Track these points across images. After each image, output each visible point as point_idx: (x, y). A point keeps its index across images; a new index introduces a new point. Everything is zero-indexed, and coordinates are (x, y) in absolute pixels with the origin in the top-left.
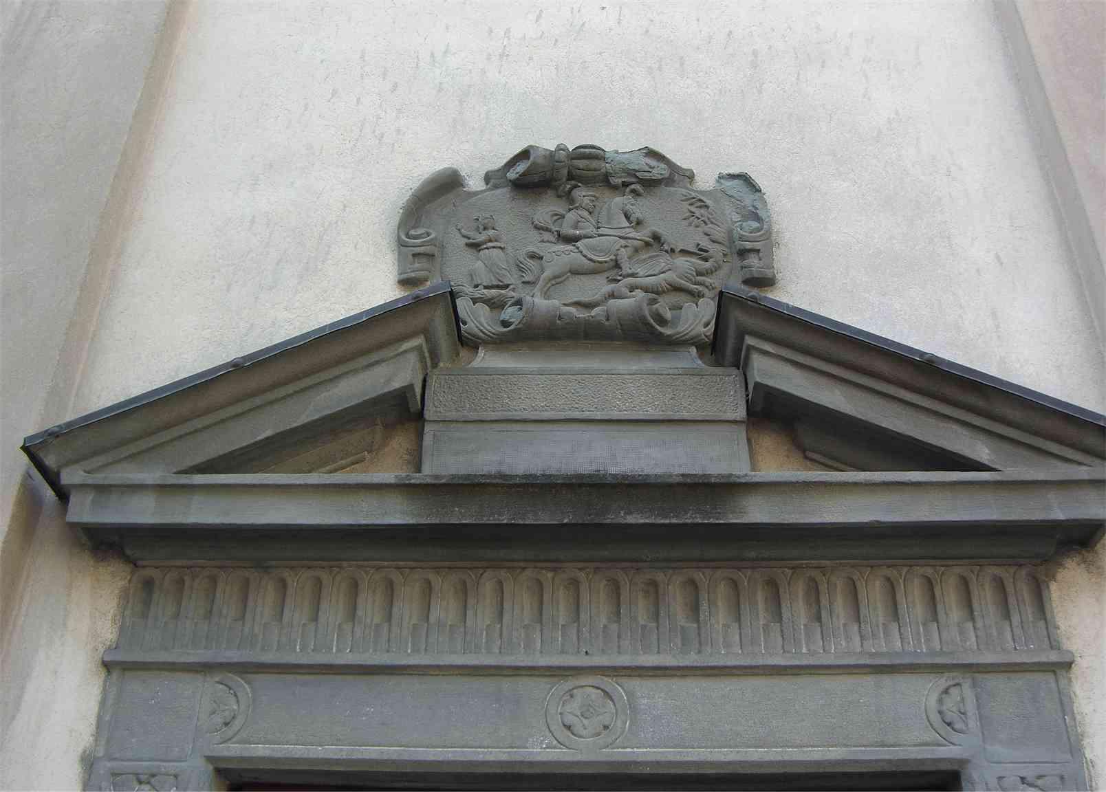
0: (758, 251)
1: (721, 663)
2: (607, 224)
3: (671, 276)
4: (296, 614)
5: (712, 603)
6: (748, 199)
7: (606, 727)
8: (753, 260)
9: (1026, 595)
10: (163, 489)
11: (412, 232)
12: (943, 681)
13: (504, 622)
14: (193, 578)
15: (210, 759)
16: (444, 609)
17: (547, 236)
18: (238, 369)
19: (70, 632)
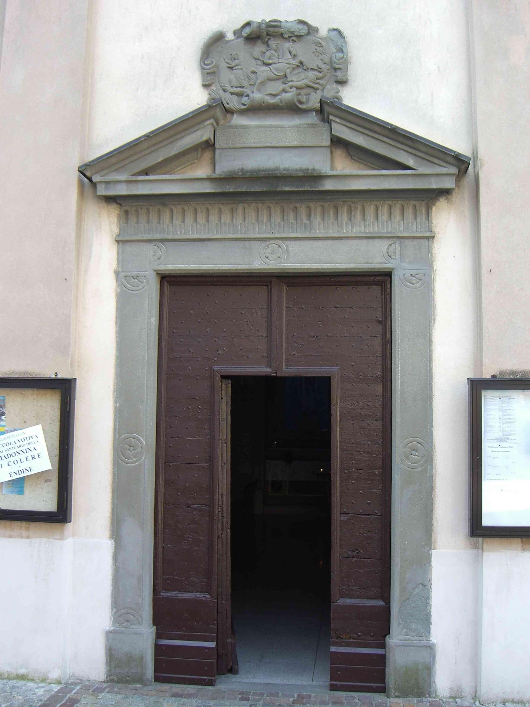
0: (341, 69)
1: (316, 236)
2: (282, 57)
3: (306, 82)
4: (177, 221)
5: (315, 215)
6: (340, 42)
7: (279, 257)
8: (339, 73)
9: (424, 211)
10: (128, 182)
11: (206, 62)
12: (389, 242)
13: (246, 222)
14: (142, 209)
15: (155, 271)
16: (226, 218)
17: (259, 63)
18: (148, 137)
19: (103, 231)
